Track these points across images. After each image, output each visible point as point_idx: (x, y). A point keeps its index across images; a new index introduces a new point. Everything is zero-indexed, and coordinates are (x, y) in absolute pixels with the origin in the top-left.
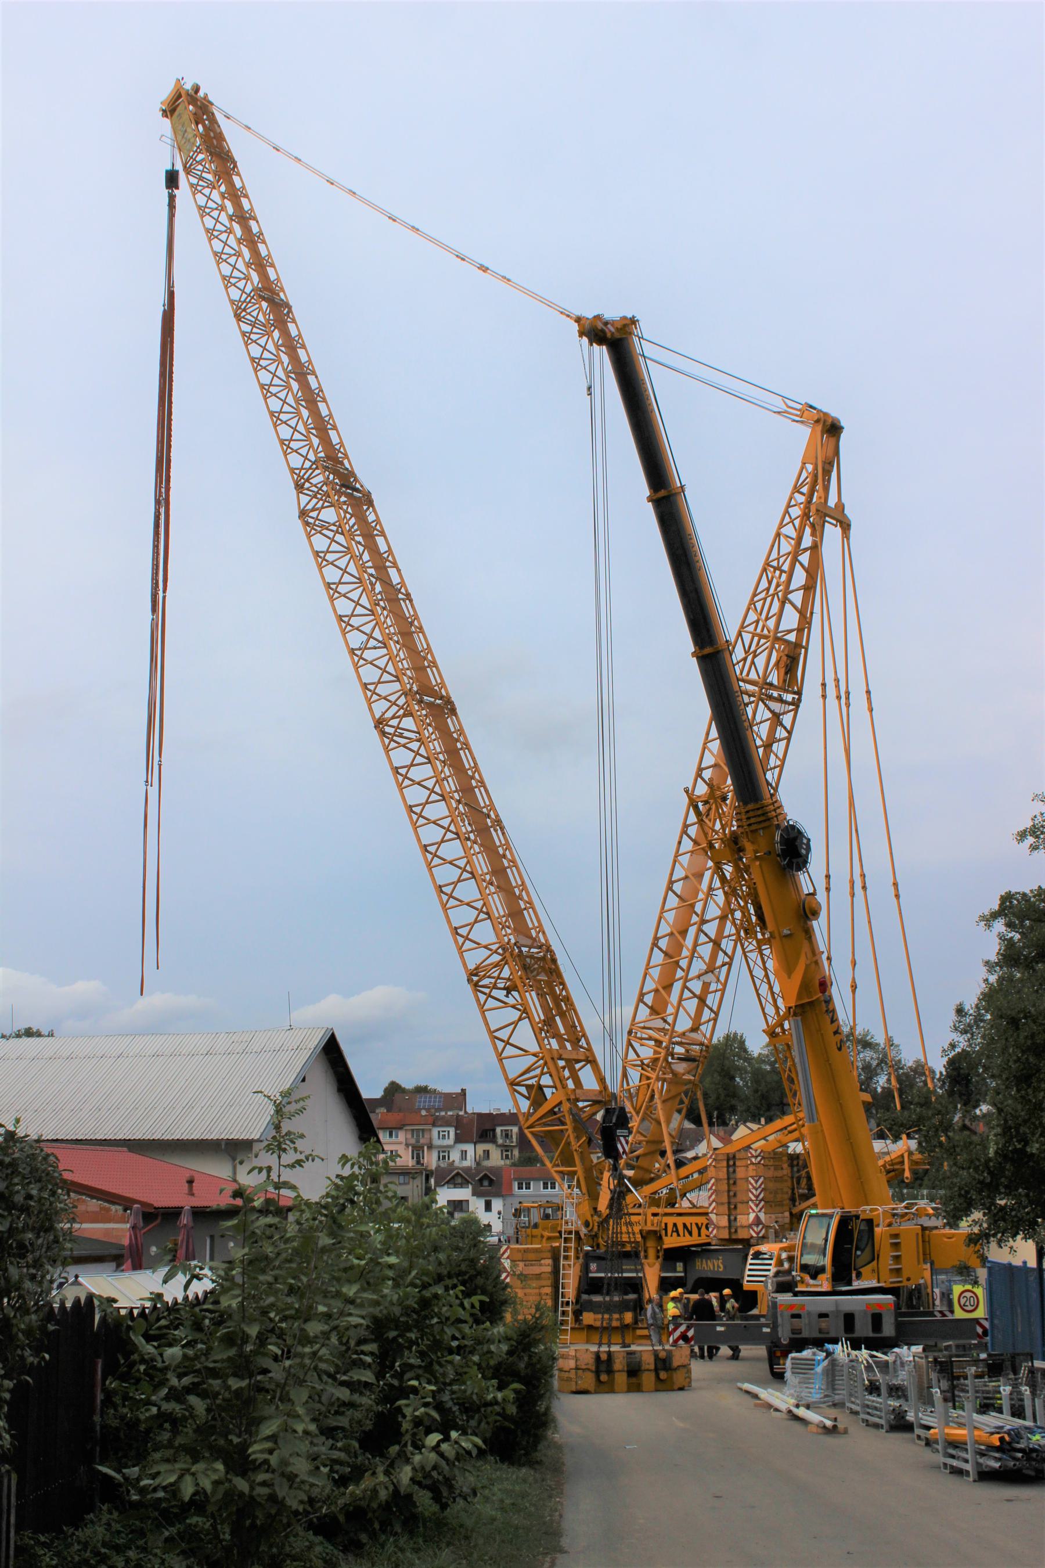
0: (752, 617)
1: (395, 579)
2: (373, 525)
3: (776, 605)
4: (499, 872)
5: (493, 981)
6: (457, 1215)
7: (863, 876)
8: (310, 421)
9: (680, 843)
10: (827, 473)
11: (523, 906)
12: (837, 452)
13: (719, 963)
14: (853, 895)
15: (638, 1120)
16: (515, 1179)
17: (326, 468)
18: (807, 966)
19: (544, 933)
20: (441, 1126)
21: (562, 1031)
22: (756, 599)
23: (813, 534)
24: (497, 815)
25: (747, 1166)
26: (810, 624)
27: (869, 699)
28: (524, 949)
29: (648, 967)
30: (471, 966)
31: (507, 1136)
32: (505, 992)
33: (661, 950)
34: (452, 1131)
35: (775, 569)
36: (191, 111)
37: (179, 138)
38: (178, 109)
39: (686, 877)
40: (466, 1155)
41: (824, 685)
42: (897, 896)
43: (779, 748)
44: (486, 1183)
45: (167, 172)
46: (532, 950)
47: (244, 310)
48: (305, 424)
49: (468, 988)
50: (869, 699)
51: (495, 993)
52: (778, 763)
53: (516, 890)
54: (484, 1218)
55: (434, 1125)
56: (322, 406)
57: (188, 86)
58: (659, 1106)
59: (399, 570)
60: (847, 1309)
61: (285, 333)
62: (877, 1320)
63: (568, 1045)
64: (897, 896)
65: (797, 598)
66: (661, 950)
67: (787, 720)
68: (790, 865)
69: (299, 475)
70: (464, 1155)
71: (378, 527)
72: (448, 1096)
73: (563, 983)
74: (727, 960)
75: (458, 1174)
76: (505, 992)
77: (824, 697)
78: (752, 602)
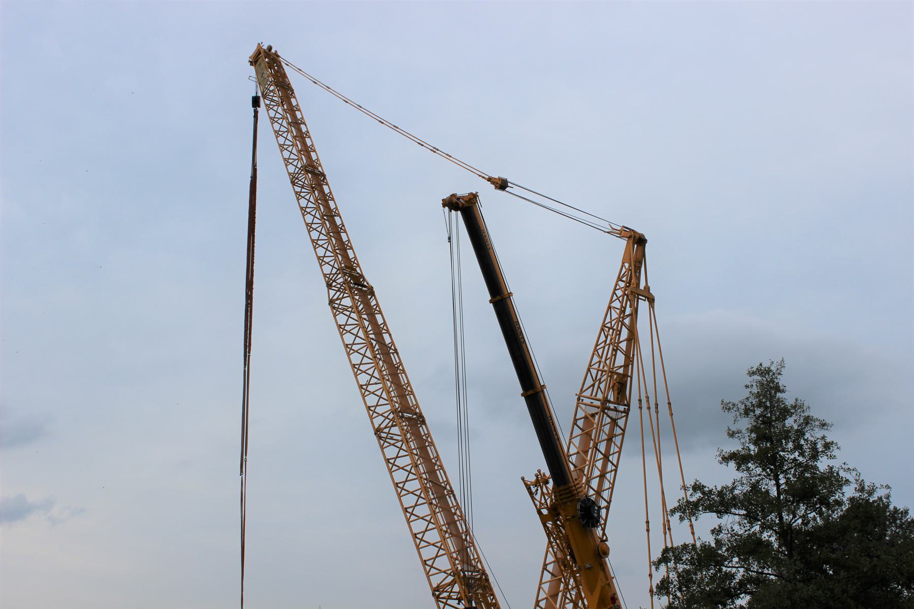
0: (596, 359)
18: (603, 588)
26: (633, 362)
27: (670, 408)
30: (435, 585)
35: (609, 329)
36: (267, 62)
43: (617, 440)
47: (334, 281)
49: (433, 599)
50: (670, 408)
51: (449, 602)
57: (265, 47)
59: (390, 335)
67: (621, 422)
68: (587, 524)
73: (493, 594)
77: (641, 408)
78: (596, 350)
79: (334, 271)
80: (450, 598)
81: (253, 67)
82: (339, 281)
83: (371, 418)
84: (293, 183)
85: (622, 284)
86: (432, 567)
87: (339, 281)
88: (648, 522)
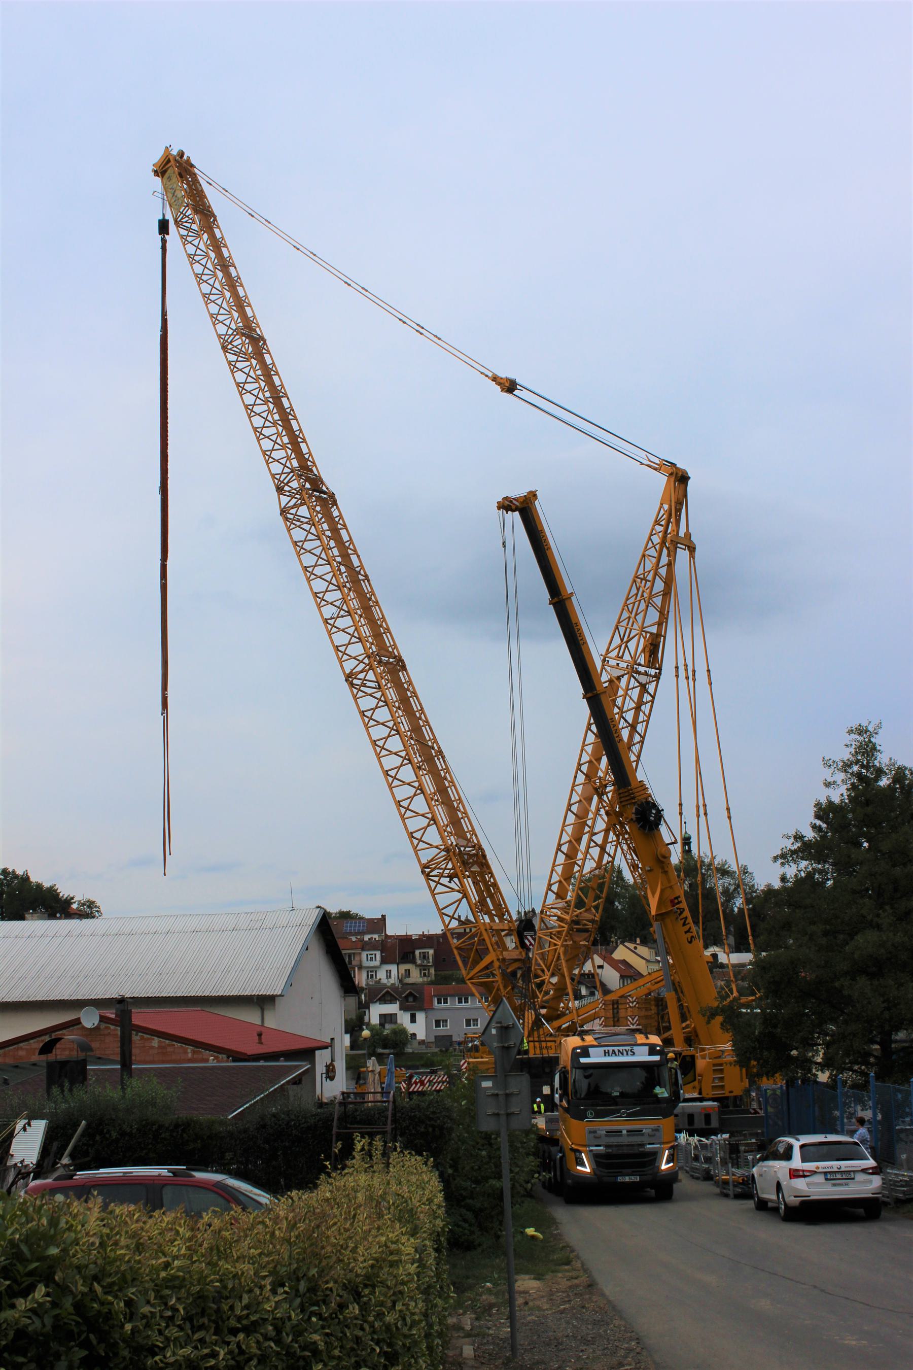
0: (626, 614)
1: (356, 563)
2: (337, 519)
3: (643, 606)
4: (442, 790)
5: (441, 871)
6: (387, 1026)
7: (705, 805)
8: (231, 300)
9: (575, 777)
10: (678, 511)
11: (447, 785)
12: (685, 495)
13: (605, 862)
14: (698, 816)
15: (549, 974)
16: (435, 996)
17: (243, 335)
19: (476, 836)
20: (369, 950)
21: (492, 908)
22: (628, 602)
23: (669, 555)
24: (439, 748)
25: (627, 1009)
26: (667, 619)
27: (709, 676)
28: (462, 849)
29: (554, 865)
30: (348, 672)
31: (424, 957)
32: (448, 879)
33: (563, 852)
34: (378, 953)
35: (642, 580)
36: (176, 170)
37: (170, 195)
38: (169, 171)
39: (580, 801)
40: (389, 974)
41: (677, 668)
42: (729, 817)
43: (646, 708)
44: (411, 999)
45: (160, 221)
46: (467, 849)
47: (230, 343)
48: (228, 302)
50: (709, 676)
51: (362, 688)
52: (646, 718)
53: (442, 773)
54: (411, 1028)
55: (363, 949)
56: (240, 289)
57: (175, 152)
58: (564, 965)
59: (358, 556)
60: (690, 1111)
61: (212, 236)
62: (708, 1117)
63: (496, 918)
64: (729, 817)
65: (658, 601)
66: (563, 852)
67: (651, 688)
69: (279, 480)
70: (389, 973)
71: (341, 522)
72: (371, 921)
73: (491, 873)
74: (610, 859)
75: (387, 992)
76: (448, 879)
77: (677, 676)
78: (626, 605)
79: (230, 332)
80: (441, 876)
81: (159, 179)
82: (235, 344)
83: (341, 662)
84: (224, 348)
85: (659, 528)
86: (407, 809)
87: (235, 344)
88: (681, 805)
